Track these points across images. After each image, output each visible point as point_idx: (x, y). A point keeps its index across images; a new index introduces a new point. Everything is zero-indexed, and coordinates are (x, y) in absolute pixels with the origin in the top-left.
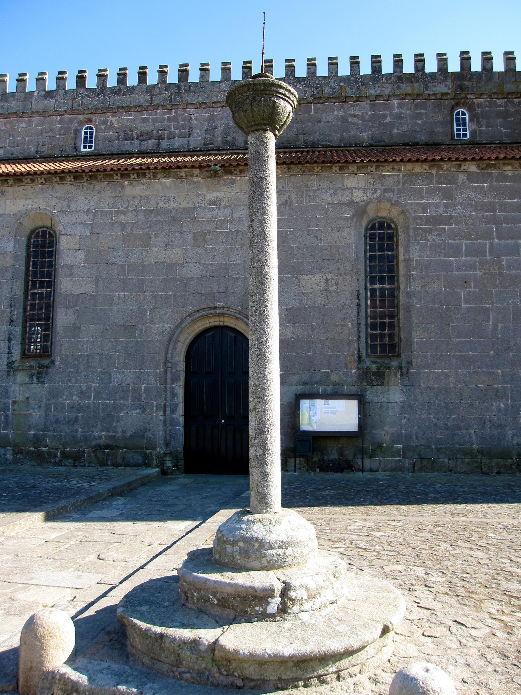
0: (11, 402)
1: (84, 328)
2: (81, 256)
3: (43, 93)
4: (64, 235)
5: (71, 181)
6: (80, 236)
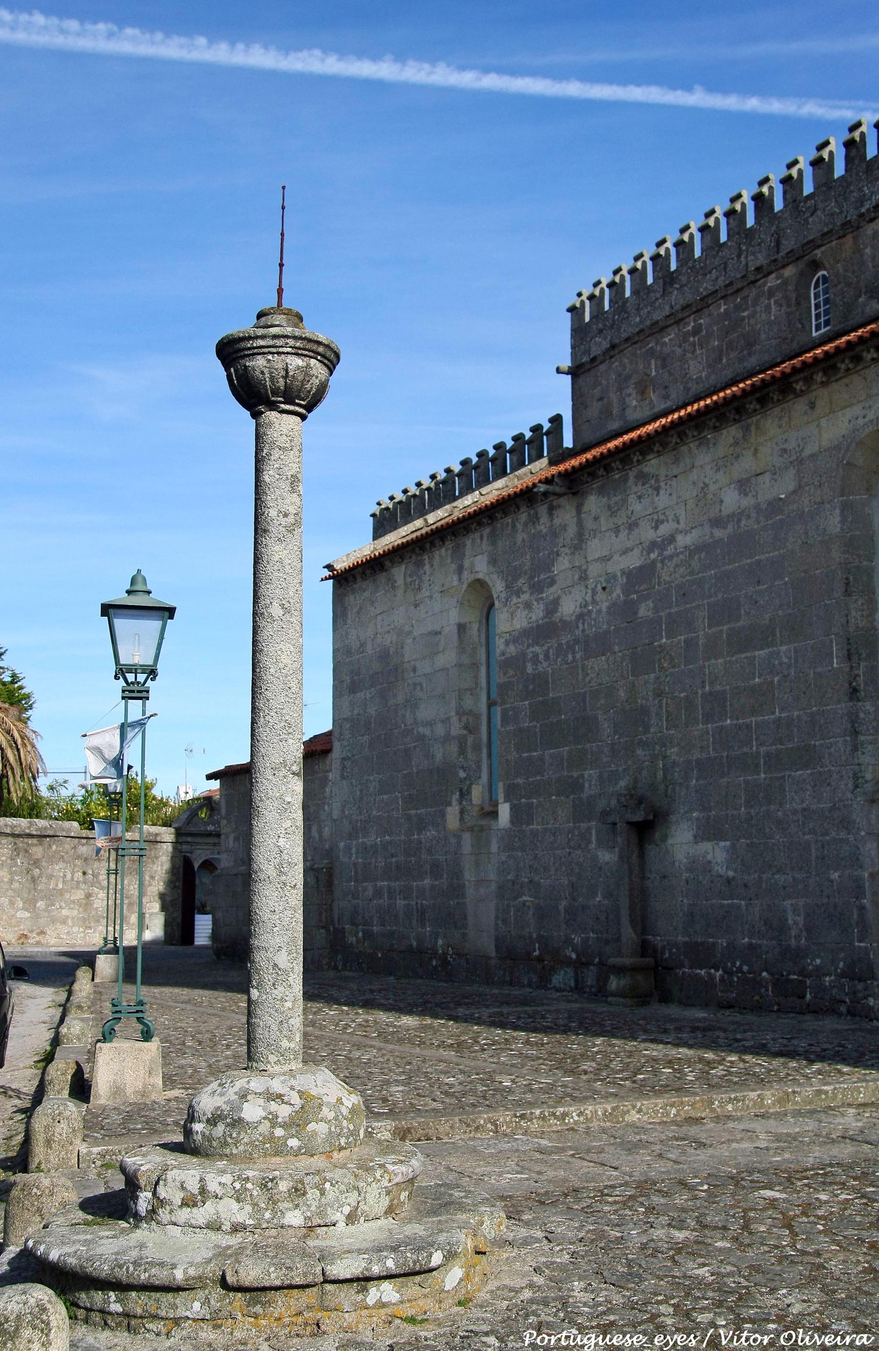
0: (866, 875)
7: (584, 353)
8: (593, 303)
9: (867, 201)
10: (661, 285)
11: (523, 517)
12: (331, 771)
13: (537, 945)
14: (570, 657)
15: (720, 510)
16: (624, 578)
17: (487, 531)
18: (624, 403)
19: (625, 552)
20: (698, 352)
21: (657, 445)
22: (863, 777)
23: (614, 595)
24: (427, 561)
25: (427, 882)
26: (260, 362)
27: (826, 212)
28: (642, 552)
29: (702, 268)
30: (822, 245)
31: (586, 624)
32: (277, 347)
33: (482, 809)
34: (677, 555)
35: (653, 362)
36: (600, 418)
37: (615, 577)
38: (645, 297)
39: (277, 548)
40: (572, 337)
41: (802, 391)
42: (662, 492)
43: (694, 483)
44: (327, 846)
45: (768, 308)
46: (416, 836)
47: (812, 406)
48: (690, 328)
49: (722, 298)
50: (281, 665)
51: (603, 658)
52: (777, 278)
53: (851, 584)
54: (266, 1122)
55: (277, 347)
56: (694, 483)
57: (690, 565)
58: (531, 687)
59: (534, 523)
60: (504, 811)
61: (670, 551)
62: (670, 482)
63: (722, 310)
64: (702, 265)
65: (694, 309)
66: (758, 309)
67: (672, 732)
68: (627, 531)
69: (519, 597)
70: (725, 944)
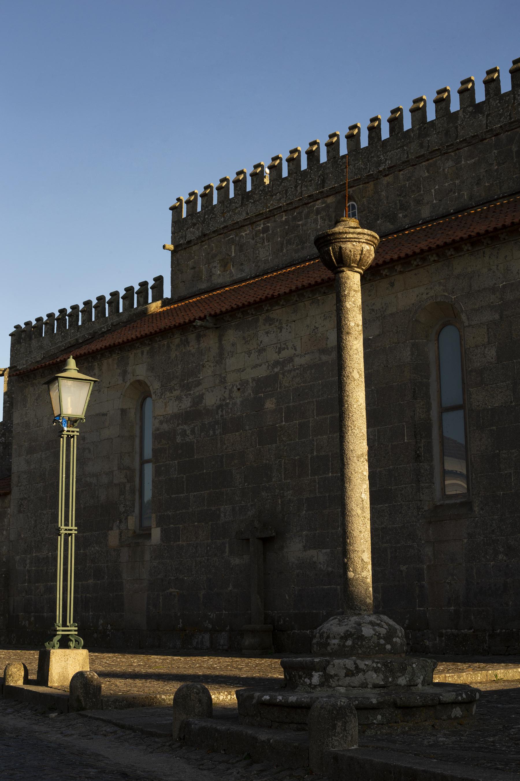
0: (425, 567)
1: (504, 455)
2: (492, 353)
3: (470, 109)
4: (469, 326)
5: (468, 250)
6: (487, 325)
7: (182, 237)
8: (189, 205)
9: (382, 163)
10: (240, 199)
11: (177, 341)
12: (9, 507)
13: (181, 620)
14: (211, 432)
15: (327, 344)
16: (254, 383)
17: (146, 349)
18: (211, 272)
19: (255, 366)
20: (266, 244)
21: (283, 301)
22: (423, 508)
23: (246, 394)
24: (96, 367)
25: (91, 581)
26: (349, 245)
27: (356, 167)
28: (268, 367)
29: (270, 191)
30: (353, 187)
31: (224, 412)
32: (359, 239)
33: (135, 532)
34: (295, 370)
35: (233, 247)
36: (193, 281)
37: (247, 382)
38: (228, 205)
39: (355, 342)
40: (172, 226)
41: (386, 275)
42: (284, 330)
43: (308, 326)
44: (4, 559)
45: (316, 221)
46: (82, 551)
47: (392, 285)
48: (261, 228)
49: (285, 211)
50: (359, 404)
51: (237, 434)
52: (323, 203)
53: (417, 392)
54: (376, 636)
55: (359, 239)
56: (308, 326)
57: (304, 377)
58: (180, 452)
59: (185, 346)
60: (156, 534)
61: (289, 367)
62: (289, 325)
63: (284, 219)
64: (270, 189)
65: (265, 217)
66: (309, 220)
67: (288, 481)
68: (257, 353)
69: (172, 393)
70: (325, 614)
